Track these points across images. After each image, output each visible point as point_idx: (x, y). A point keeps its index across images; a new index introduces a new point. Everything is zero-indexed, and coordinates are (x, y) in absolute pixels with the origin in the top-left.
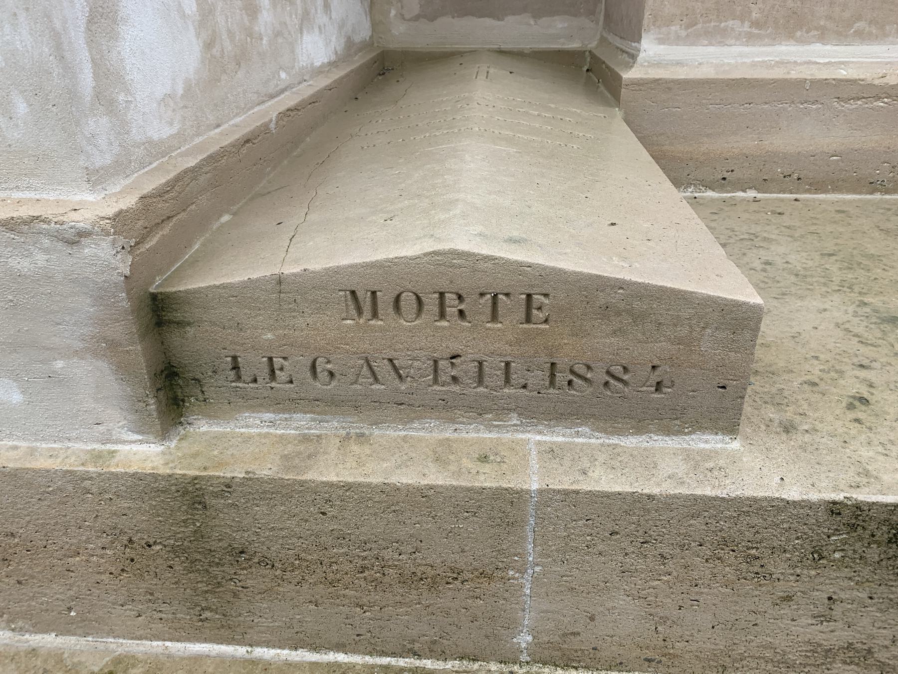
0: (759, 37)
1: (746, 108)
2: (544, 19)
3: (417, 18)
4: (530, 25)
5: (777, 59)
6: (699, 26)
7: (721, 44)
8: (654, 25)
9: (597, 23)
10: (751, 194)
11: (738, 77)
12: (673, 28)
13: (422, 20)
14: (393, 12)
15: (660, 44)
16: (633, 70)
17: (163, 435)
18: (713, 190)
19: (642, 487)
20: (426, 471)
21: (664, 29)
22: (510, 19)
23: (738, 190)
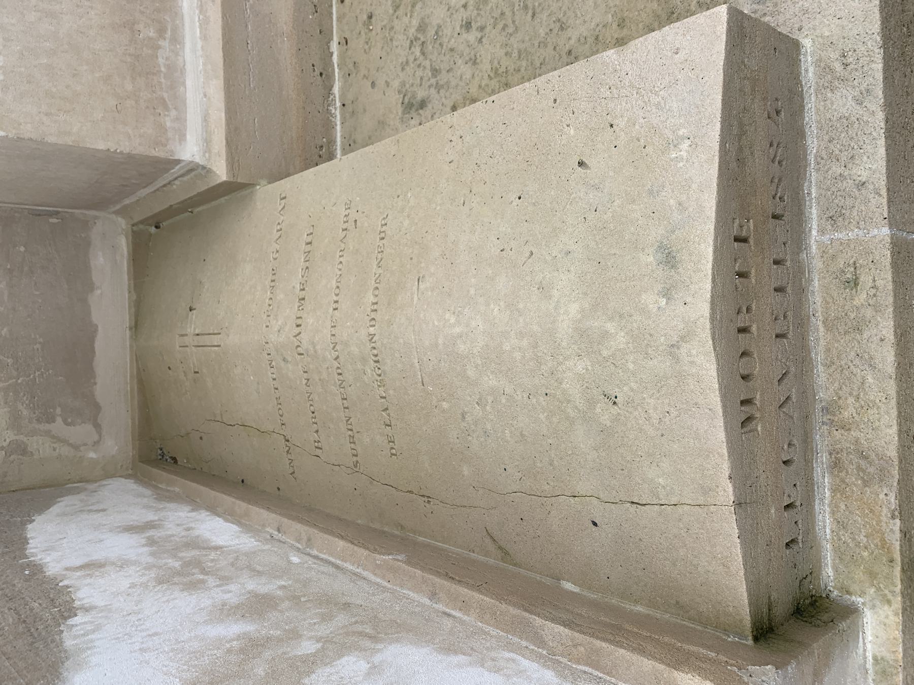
0: (175, 30)
1: (252, 47)
2: (94, 279)
3: (97, 426)
4: (101, 294)
5: (197, 12)
6: (165, 95)
7: (183, 71)
8: (166, 146)
9: (96, 217)
10: (334, 47)
11: (221, 54)
12: (168, 124)
13: (99, 421)
14: (92, 455)
15: (185, 140)
16: (214, 169)
17: (851, 612)
18: (332, 86)
19: (878, 129)
20: (876, 339)
21: (170, 134)
22: (96, 317)
23: (331, 60)
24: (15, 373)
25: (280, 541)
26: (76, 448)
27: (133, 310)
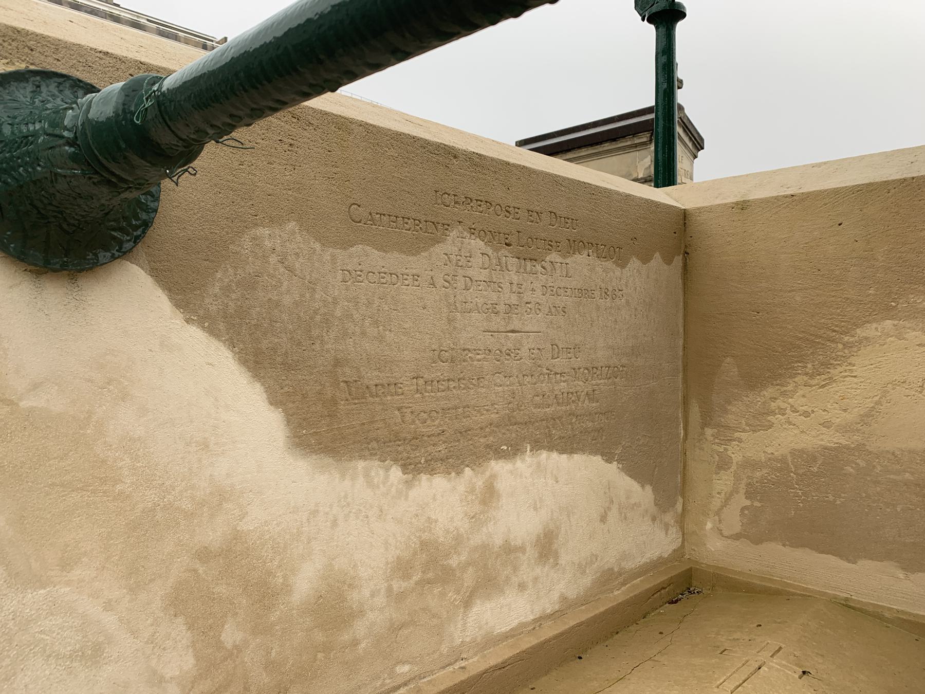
3: (737, 537)
14: (709, 525)
24: (801, 472)
25: (449, 665)
26: (718, 513)
27: (871, 609)
